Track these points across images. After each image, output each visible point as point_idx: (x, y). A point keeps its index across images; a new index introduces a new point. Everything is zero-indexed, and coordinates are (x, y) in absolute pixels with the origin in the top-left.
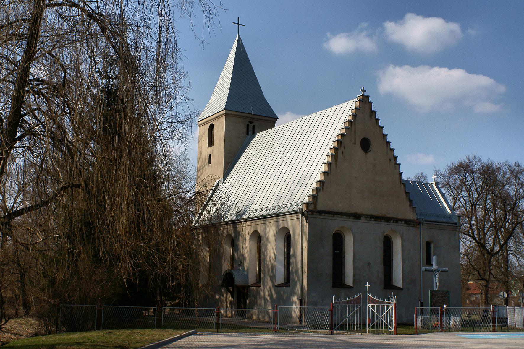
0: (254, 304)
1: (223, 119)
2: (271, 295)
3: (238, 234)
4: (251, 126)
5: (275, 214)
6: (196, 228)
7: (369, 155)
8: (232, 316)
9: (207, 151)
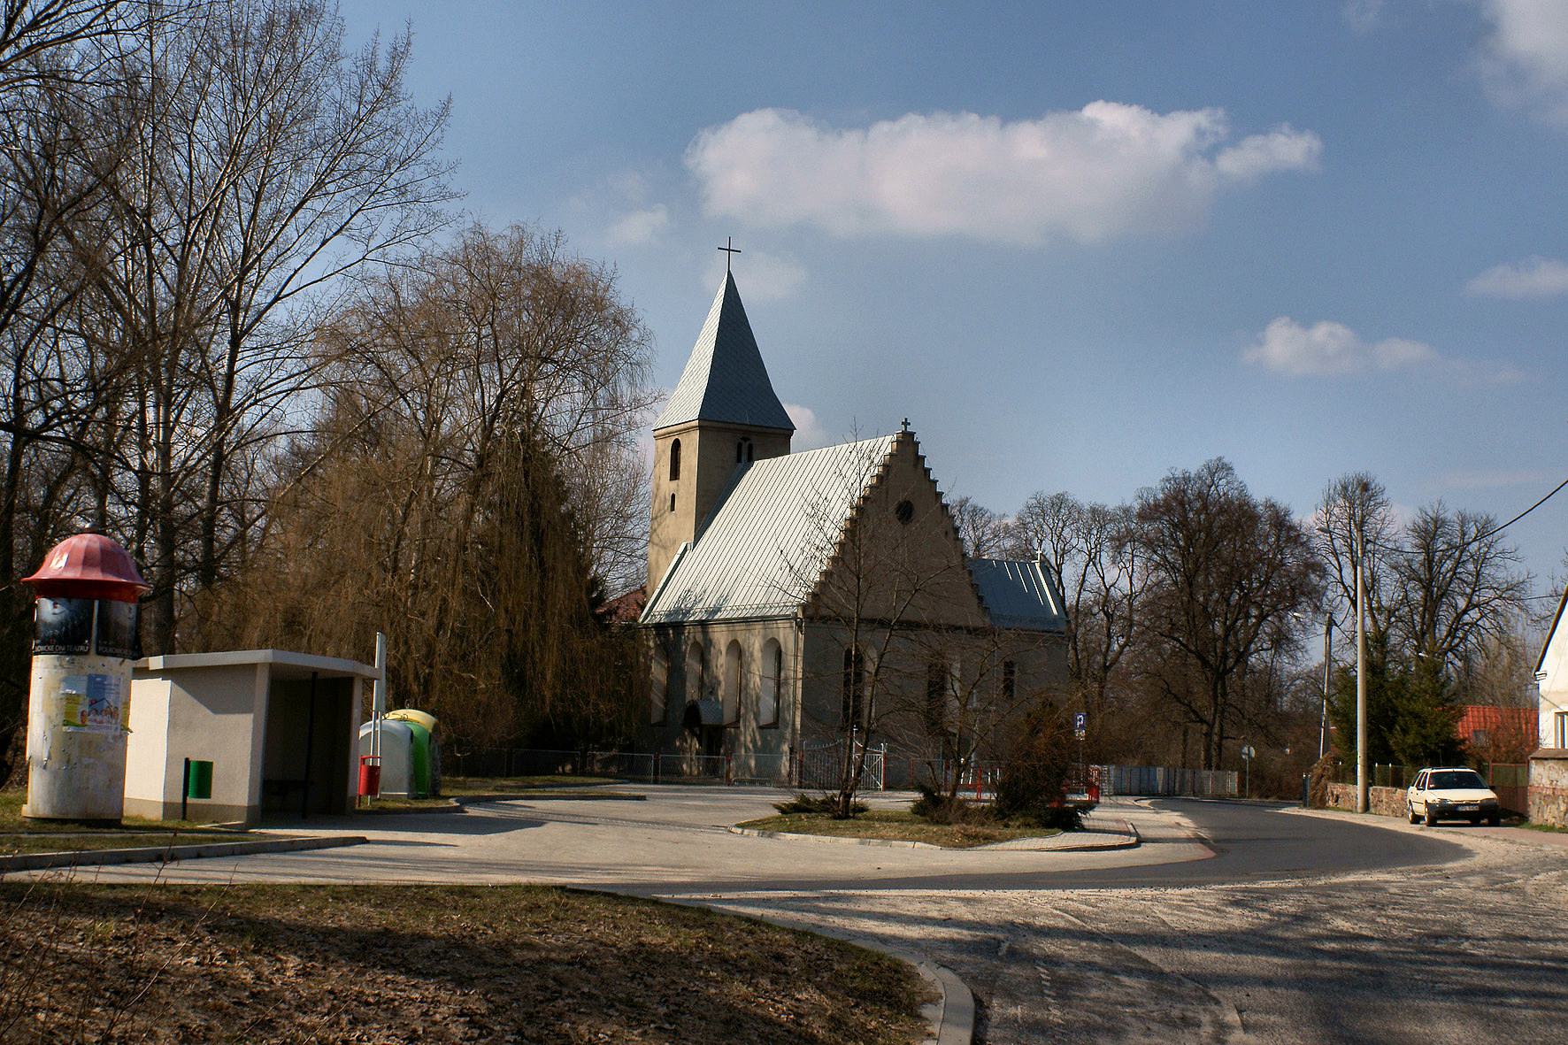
0: (730, 754)
1: (696, 435)
2: (754, 741)
3: (709, 642)
4: (745, 446)
5: (762, 617)
6: (646, 627)
7: (913, 527)
8: (699, 774)
9: (668, 486)
